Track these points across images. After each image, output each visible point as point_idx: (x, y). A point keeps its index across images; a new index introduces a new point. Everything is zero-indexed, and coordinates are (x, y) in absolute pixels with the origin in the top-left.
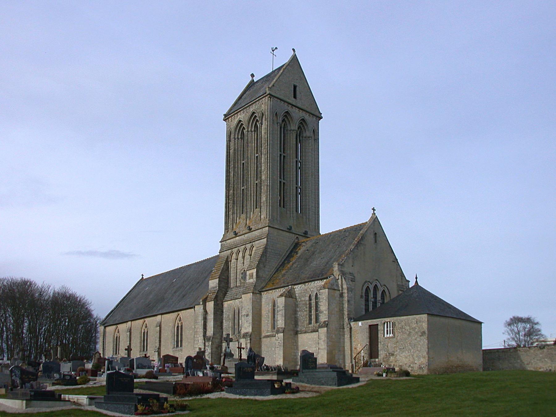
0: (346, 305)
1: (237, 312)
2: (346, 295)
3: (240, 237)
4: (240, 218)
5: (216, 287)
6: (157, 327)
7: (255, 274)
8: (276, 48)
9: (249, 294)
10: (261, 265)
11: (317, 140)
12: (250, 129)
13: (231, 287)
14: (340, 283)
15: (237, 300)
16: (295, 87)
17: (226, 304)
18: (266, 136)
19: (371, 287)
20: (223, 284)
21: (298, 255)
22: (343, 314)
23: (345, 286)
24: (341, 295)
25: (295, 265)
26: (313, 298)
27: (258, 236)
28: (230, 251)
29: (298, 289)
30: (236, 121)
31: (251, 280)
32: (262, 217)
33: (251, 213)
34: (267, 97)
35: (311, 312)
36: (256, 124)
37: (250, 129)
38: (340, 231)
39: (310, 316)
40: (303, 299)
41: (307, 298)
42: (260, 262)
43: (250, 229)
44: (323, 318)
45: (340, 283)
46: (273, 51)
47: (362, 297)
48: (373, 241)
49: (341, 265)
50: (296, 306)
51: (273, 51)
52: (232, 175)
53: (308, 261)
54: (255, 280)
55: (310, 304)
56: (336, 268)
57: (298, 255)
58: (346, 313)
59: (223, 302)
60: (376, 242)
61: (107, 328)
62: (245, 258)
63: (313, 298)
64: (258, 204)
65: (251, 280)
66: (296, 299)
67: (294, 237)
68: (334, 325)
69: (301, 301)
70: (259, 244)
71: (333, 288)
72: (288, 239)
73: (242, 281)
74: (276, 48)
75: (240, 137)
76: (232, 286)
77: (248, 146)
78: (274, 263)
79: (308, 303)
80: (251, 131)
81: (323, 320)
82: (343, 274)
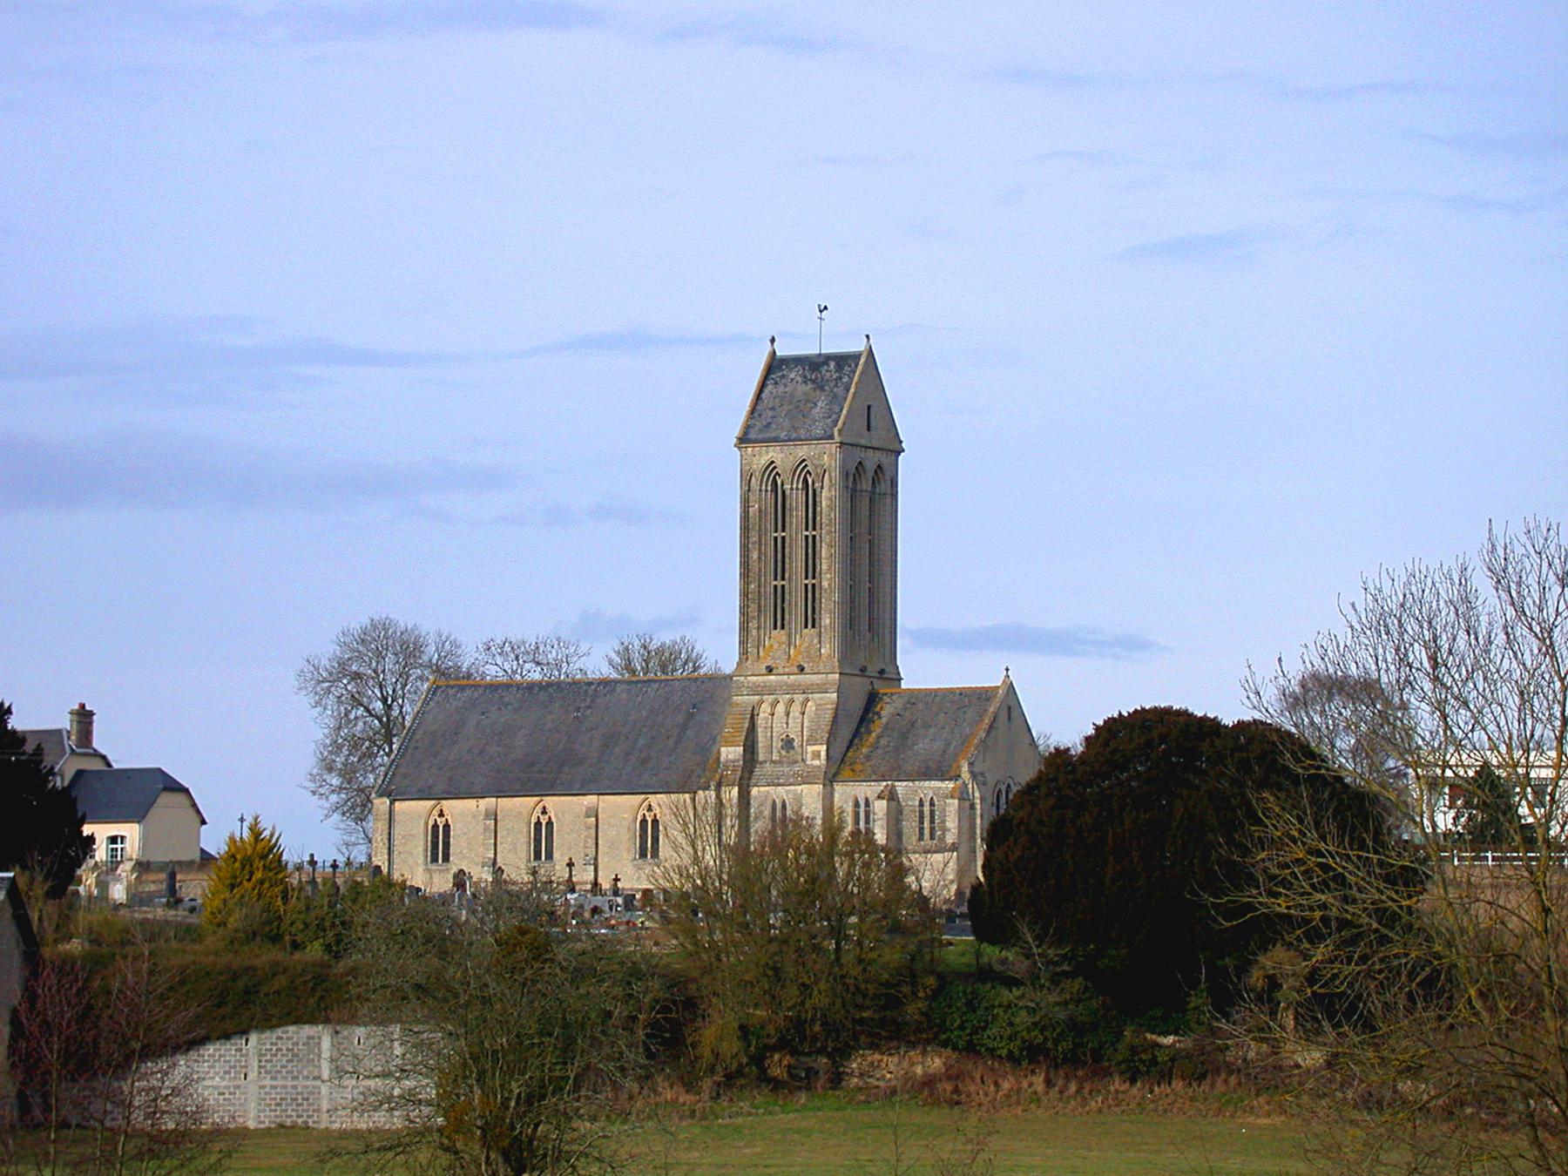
0: (978, 821)
1: (779, 806)
2: (978, 807)
3: (780, 678)
4: (770, 638)
5: (738, 761)
6: (588, 817)
7: (823, 754)
8: (826, 308)
9: (816, 786)
10: (832, 739)
11: (895, 496)
12: (795, 486)
13: (760, 759)
14: (970, 790)
15: (780, 788)
16: (869, 407)
17: (754, 791)
18: (833, 515)
19: (1004, 788)
20: (748, 756)
21: (884, 720)
22: (975, 833)
23: (977, 794)
24: (972, 806)
25: (883, 742)
26: (927, 804)
27: (817, 684)
28: (757, 697)
29: (901, 787)
30: (764, 460)
31: (817, 762)
32: (823, 651)
33: (798, 637)
34: (834, 446)
35: (923, 823)
36: (805, 477)
37: (795, 486)
38: (951, 691)
39: (921, 829)
40: (910, 803)
41: (917, 803)
42: (831, 733)
43: (802, 669)
44: (950, 839)
45: (970, 790)
46: (821, 311)
47: (993, 804)
48: (1006, 719)
49: (971, 764)
50: (900, 812)
51: (821, 311)
52: (755, 555)
53: (907, 738)
54: (824, 762)
55: (921, 813)
56: (965, 768)
57: (884, 720)
58: (978, 831)
59: (749, 786)
60: (1009, 719)
61: (397, 803)
62: (791, 715)
63: (927, 804)
64: (811, 620)
65: (817, 762)
66: (899, 801)
67: (868, 681)
68: (964, 848)
69: (907, 805)
70: (821, 699)
71: (963, 796)
72: (861, 687)
73: (784, 753)
74: (826, 308)
75: (769, 488)
76: (761, 757)
77: (791, 515)
78: (846, 733)
79: (917, 809)
80: (797, 489)
81: (951, 841)
82: (974, 776)
